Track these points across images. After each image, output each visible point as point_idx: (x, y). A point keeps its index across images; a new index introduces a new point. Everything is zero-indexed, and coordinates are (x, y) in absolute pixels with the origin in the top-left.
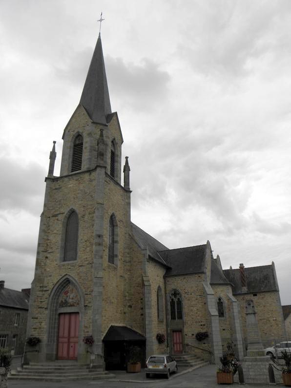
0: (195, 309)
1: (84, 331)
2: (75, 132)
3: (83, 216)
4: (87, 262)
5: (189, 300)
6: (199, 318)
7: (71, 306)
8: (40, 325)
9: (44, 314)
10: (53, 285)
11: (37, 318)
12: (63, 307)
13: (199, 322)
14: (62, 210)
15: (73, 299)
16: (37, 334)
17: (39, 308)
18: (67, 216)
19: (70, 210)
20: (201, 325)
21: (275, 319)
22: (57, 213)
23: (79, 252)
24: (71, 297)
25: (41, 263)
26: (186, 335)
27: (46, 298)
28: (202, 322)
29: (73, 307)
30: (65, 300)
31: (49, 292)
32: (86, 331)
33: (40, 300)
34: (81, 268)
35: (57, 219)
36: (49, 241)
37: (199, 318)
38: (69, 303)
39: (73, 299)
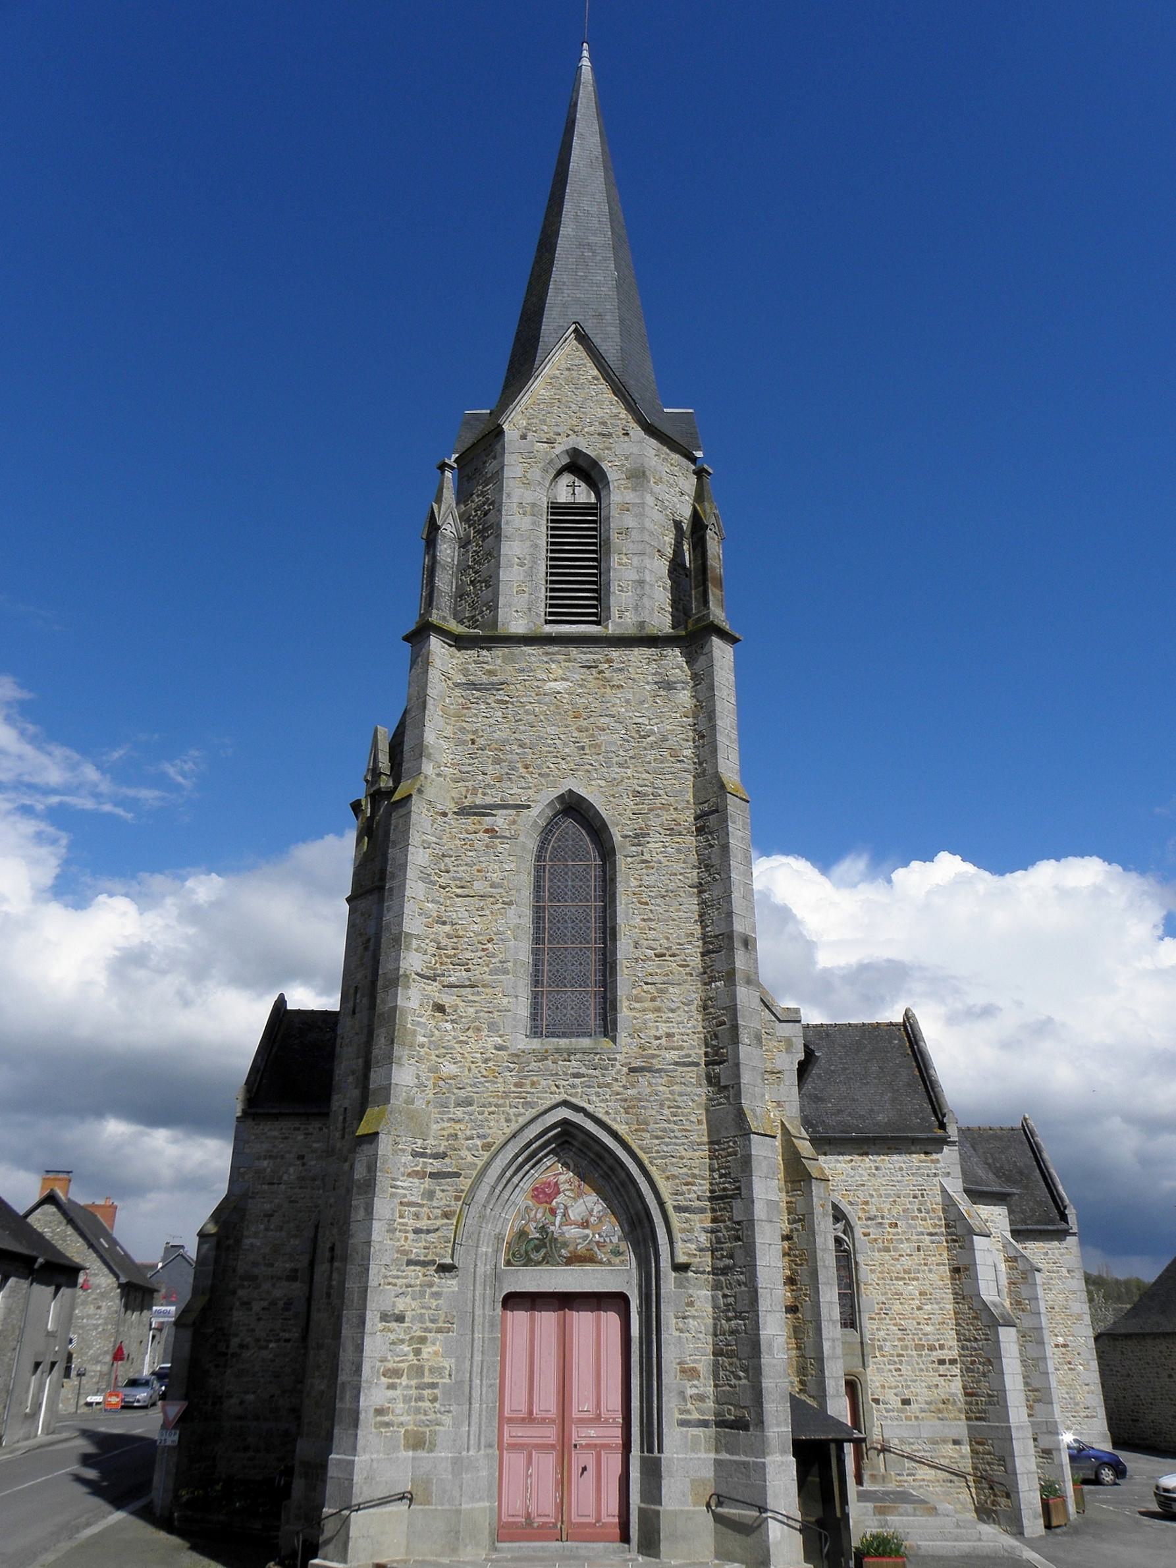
0: (913, 1288)
1: (682, 1393)
2: (559, 449)
3: (639, 837)
4: (672, 1056)
5: (887, 1250)
6: (929, 1329)
7: (575, 1259)
8: (417, 1352)
9: (437, 1295)
10: (487, 1147)
11: (400, 1319)
12: (528, 1262)
13: (932, 1348)
14: (514, 792)
15: (585, 1224)
16: (896, 1441)
17: (410, 1263)
18: (542, 823)
19: (561, 798)
20: (942, 1362)
21: (1061, 1340)
22: (489, 800)
23: (625, 1004)
24: (573, 1215)
25: (414, 1033)
26: (877, 1401)
27: (446, 1215)
28: (942, 1347)
29: (588, 1268)
30: (543, 1229)
31: (465, 1183)
32: (691, 1392)
33: (412, 1223)
34: (643, 1079)
35: (490, 831)
36: (447, 928)
37: (929, 1329)
38: (565, 1245)
39: (585, 1224)
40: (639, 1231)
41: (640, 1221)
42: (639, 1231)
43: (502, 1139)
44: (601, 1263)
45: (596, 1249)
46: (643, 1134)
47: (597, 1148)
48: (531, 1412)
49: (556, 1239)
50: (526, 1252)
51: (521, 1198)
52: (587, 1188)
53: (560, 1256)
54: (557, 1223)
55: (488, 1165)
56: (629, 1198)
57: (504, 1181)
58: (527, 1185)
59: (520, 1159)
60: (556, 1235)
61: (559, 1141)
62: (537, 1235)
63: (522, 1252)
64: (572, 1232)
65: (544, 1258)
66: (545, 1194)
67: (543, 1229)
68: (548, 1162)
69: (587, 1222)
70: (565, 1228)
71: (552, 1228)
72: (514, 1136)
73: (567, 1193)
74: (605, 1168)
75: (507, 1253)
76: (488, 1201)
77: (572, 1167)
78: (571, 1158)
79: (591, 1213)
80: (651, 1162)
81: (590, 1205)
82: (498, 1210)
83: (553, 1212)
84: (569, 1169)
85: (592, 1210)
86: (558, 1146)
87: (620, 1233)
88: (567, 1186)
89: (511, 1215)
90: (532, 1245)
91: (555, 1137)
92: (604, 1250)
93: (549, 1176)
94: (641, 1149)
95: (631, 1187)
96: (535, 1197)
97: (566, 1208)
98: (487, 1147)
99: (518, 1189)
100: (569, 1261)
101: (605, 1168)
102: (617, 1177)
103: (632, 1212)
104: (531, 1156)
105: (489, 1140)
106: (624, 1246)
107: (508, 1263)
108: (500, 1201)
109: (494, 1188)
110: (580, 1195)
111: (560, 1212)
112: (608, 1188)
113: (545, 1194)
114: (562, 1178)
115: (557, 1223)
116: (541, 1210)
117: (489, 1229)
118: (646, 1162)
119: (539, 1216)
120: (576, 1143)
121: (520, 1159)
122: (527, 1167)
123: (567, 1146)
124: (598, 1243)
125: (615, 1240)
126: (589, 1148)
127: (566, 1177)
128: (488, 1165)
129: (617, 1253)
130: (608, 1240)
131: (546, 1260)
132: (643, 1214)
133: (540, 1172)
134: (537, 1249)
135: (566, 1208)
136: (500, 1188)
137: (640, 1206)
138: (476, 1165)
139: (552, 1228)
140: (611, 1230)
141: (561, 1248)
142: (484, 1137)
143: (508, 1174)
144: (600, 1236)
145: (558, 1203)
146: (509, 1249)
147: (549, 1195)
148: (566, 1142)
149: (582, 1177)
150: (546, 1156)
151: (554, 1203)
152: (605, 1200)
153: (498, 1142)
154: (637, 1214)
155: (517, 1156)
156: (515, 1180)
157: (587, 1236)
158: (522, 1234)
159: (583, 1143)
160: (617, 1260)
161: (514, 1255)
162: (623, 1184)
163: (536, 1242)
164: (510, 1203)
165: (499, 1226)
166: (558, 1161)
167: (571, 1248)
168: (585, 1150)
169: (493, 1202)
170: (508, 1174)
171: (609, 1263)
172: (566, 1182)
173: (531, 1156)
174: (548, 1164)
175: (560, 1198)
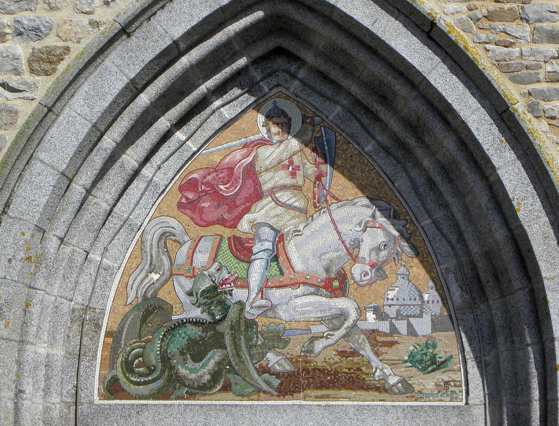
10: (44, 61)
12: (172, 385)
15: (336, 283)
29: (347, 402)
38: (277, 339)
39: (336, 283)
40: (495, 302)
41: (497, 275)
42: (495, 302)
43: (91, 40)
44: (382, 389)
45: (367, 351)
46: (514, 28)
47: (377, 69)
48: (174, 275)
49: (251, 324)
50: (165, 358)
51: (148, 206)
52: (338, 182)
53: (264, 370)
54: (255, 279)
55: (49, 112)
56: (466, 209)
57: (97, 160)
58: (163, 172)
59: (144, 99)
60: (250, 313)
61: (260, 50)
62: (196, 313)
63: (153, 357)
64: (298, 306)
65: (216, 376)
66: (216, 199)
67: (213, 296)
68: (225, 109)
69: (342, 277)
70: (276, 295)
71: (239, 294)
72: (125, 31)
73: (284, 197)
74: (395, 126)
75: (110, 361)
76: (51, 213)
77: (297, 124)
78: (295, 98)
79: (352, 251)
80: (532, 108)
81: (350, 230)
82: (80, 240)
83: (242, 249)
84: (286, 126)
85: (357, 244)
86: (255, 62)
87: (437, 308)
88: (282, 177)
89: (118, 255)
90: (180, 339)
91: (247, 37)
92: (390, 353)
93: (227, 150)
94: (504, 66)
95: (471, 178)
96: (188, 207)
97: (280, 238)
98: (44, 61)
99: (138, 185)
100: (290, 385)
101: (355, 89)
102: (432, 154)
103: (475, 249)
104: (174, 92)
105: (51, 41)
106: (447, 344)
107: (113, 389)
108: (86, 217)
109: (68, 178)
110: (320, 202)
111: (262, 248)
112: (402, 183)
113: (216, 199)
114: (268, 155)
115: (255, 279)
116: (206, 245)
117: (54, 295)
118: (520, 107)
119: (201, 258)
120: (309, 57)
121: (144, 99)
122: (163, 123)
123: (280, 62)
124: (372, 334)
125: (423, 326)
126: (348, 69)
127: (279, 153)
128: (49, 112)
129: (430, 363)
130: (402, 326)
131: (221, 381)
132: (507, 254)
133: (201, 137)
134: (196, 351)
135: (280, 238)
136: (85, 178)
137: (499, 234)
138: (13, 112)
139: (239, 294)
140: (410, 298)
141: (266, 348)
142: (37, 32)
143: (109, 142)
144: (380, 315)
145: (256, 226)
146: (113, 350)
147: (230, 203)
148: (279, 51)
149: (325, 150)
150: (221, 90)
151: (244, 225)
152: (394, 216)
153: (76, 49)
154: (489, 255)
155: (134, 89)
156: (131, 158)
157: (342, 316)
158: (152, 309)
159: (331, 54)
160: (428, 382)
161: (128, 367)
162: (447, 171)
163: (194, 332)
164: (114, 222)
165: (85, 284)
166: (257, 106)
167: (295, 348)
168: (335, 74)
169: (66, 216)
170: (109, 142)
171: (407, 389)
172: (279, 165)
173: (174, 92)
174: (228, 113)
175: (263, 211)
